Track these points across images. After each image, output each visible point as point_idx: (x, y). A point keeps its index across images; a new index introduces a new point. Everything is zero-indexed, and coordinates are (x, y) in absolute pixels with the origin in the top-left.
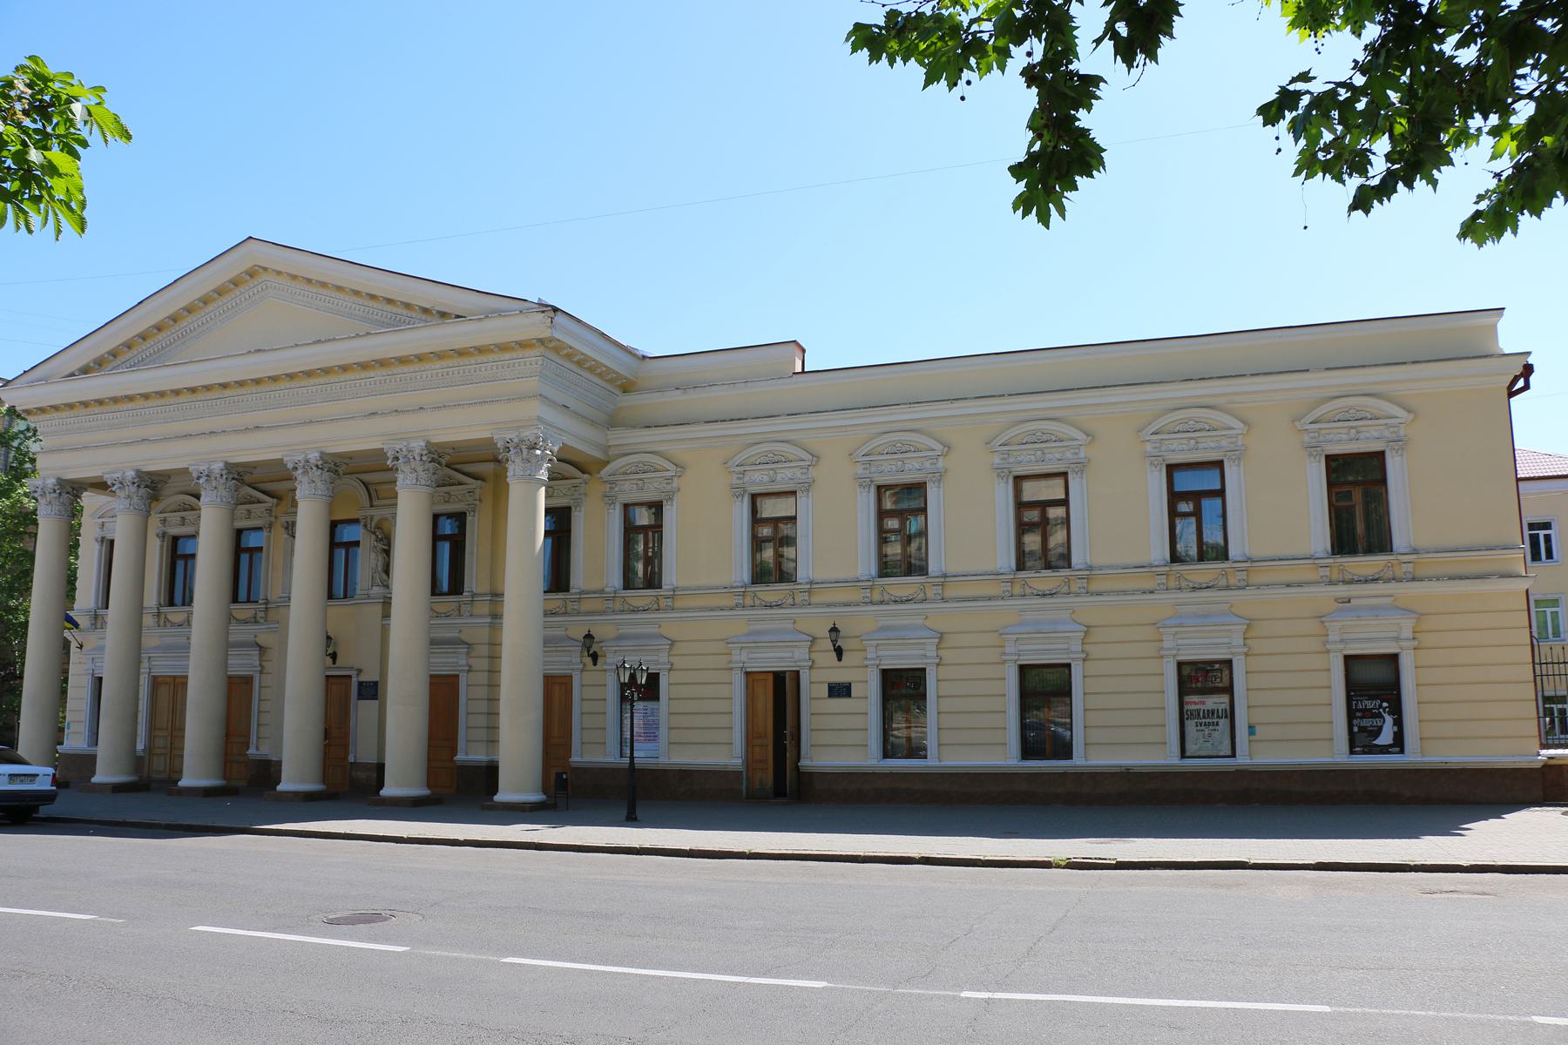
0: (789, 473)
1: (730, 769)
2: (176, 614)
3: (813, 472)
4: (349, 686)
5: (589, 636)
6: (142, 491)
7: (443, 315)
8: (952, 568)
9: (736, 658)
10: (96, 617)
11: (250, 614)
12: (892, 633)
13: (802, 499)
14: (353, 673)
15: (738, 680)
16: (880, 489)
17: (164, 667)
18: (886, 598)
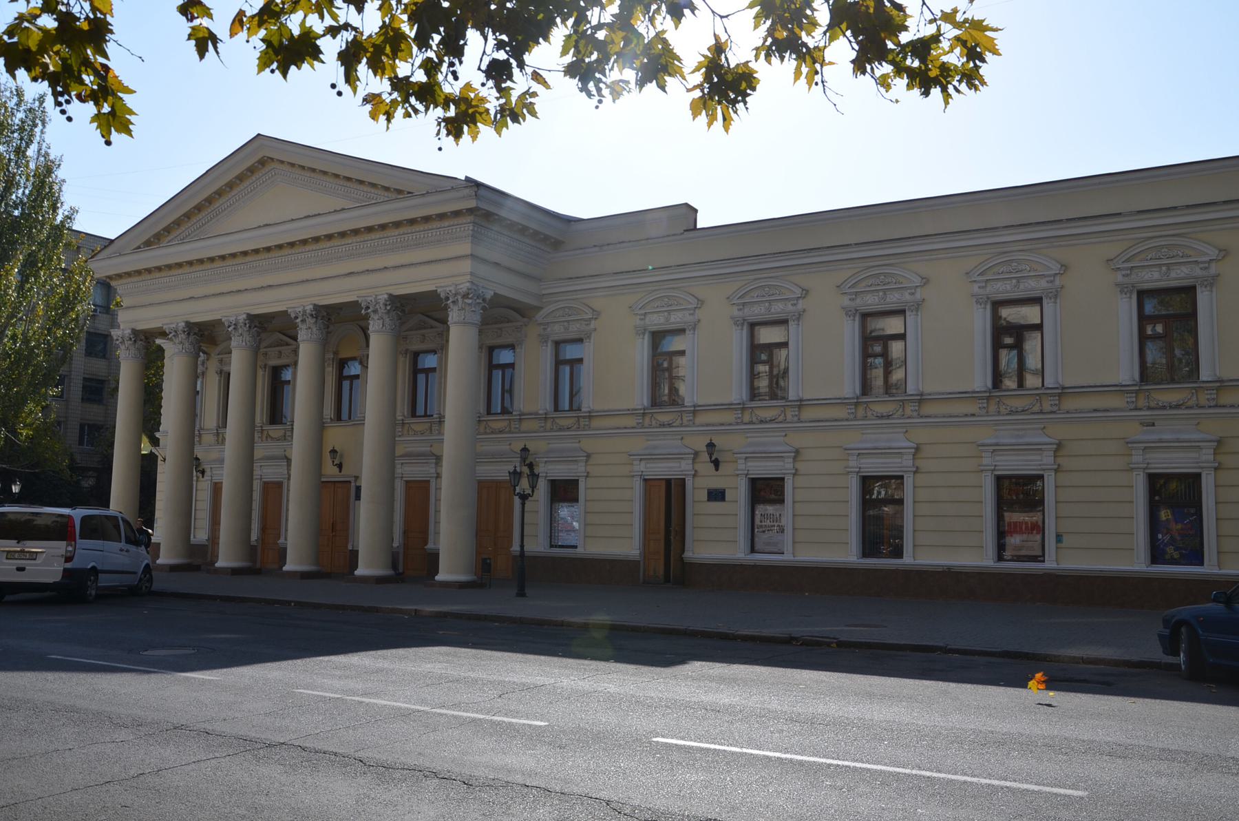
0: (680, 314)
1: (631, 558)
2: (276, 431)
3: (801, 305)
4: (349, 489)
5: (525, 450)
6: (192, 338)
7: (399, 192)
8: (929, 388)
9: (851, 463)
10: (218, 434)
11: (281, 433)
12: (754, 450)
13: (910, 317)
14: (352, 479)
15: (638, 485)
16: (1142, 295)
17: (267, 472)
18: (1152, 404)
